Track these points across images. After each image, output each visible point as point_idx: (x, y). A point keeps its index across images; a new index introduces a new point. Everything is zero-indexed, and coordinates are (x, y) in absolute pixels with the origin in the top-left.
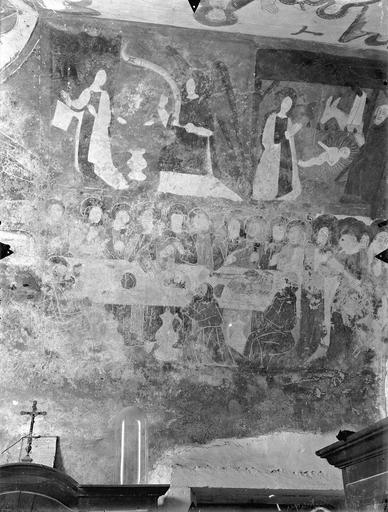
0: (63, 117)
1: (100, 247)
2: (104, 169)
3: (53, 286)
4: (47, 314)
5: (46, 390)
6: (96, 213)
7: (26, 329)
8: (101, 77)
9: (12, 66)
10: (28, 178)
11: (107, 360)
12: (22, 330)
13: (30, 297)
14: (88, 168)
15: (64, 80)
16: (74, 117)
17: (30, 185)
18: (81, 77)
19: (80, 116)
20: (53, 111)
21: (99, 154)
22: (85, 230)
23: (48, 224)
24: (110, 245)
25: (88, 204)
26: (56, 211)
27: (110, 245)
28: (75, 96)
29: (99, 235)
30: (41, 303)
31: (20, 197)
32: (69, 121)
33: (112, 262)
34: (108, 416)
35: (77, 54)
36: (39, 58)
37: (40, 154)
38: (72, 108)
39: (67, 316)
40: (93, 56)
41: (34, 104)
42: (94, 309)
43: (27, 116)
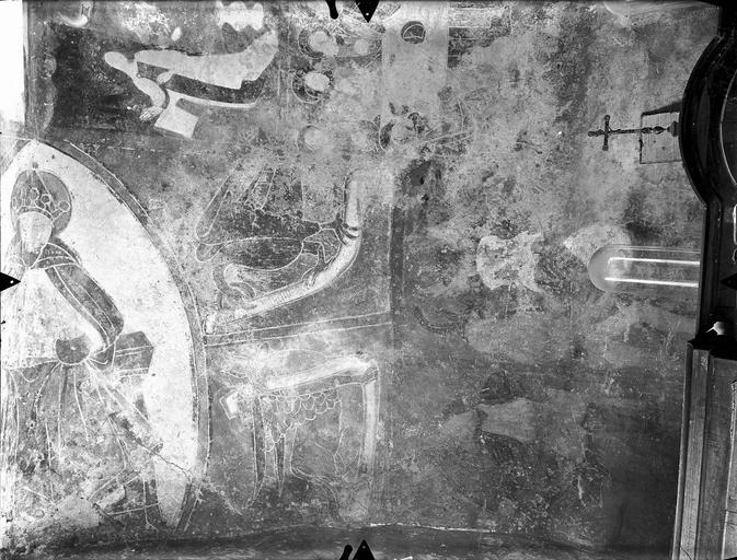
0: (176, 120)
1: (364, 75)
2: (249, 66)
3: (423, 144)
4: (462, 151)
5: (573, 144)
6: (314, 81)
7: (484, 180)
8: (114, 60)
9: (113, 185)
10: (270, 175)
11: (531, 60)
12: (485, 184)
13: (438, 175)
14: (248, 90)
15: (125, 114)
16: (178, 105)
17: (279, 173)
18: (118, 90)
19: (175, 96)
20: (169, 133)
21: (230, 72)
22: (340, 97)
23: (334, 150)
24: (361, 60)
25: (302, 91)
26: (314, 138)
27: (361, 60)
28: (147, 101)
29: (346, 76)
30: (447, 160)
31: (297, 188)
32: (183, 113)
33: (386, 58)
34: (615, 50)
35: (86, 92)
36: (96, 147)
37: (235, 158)
38: (165, 106)
39: (465, 122)
40: (86, 68)
41: (164, 160)
42: (455, 84)
43: (181, 170)
